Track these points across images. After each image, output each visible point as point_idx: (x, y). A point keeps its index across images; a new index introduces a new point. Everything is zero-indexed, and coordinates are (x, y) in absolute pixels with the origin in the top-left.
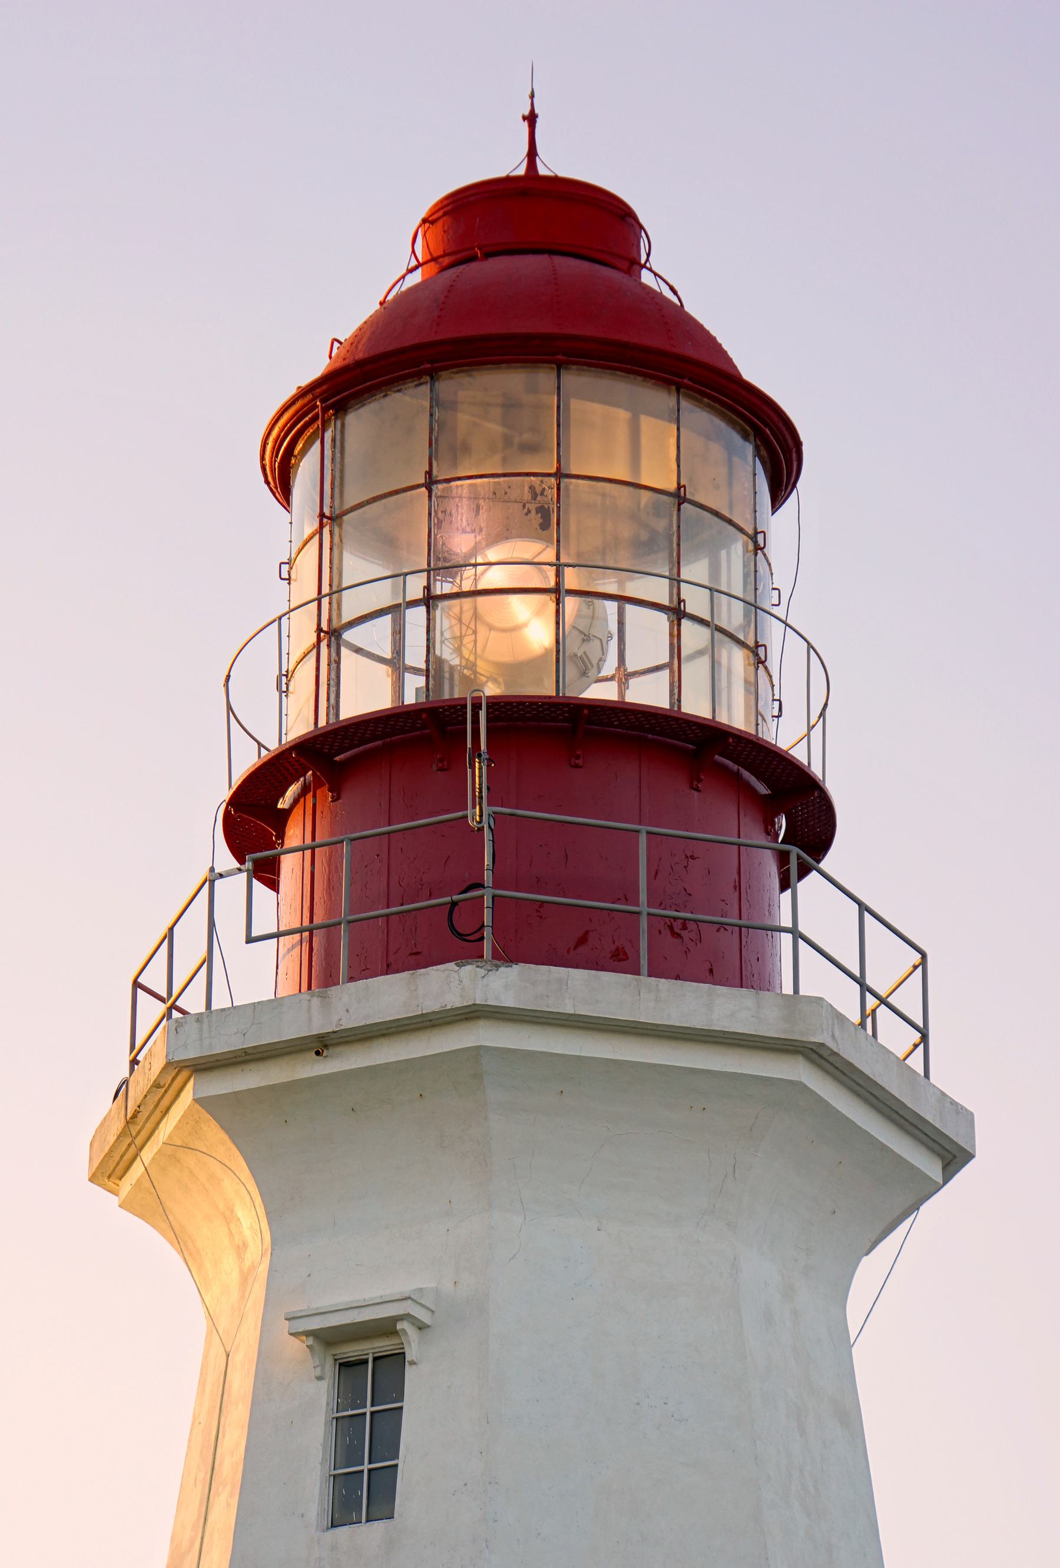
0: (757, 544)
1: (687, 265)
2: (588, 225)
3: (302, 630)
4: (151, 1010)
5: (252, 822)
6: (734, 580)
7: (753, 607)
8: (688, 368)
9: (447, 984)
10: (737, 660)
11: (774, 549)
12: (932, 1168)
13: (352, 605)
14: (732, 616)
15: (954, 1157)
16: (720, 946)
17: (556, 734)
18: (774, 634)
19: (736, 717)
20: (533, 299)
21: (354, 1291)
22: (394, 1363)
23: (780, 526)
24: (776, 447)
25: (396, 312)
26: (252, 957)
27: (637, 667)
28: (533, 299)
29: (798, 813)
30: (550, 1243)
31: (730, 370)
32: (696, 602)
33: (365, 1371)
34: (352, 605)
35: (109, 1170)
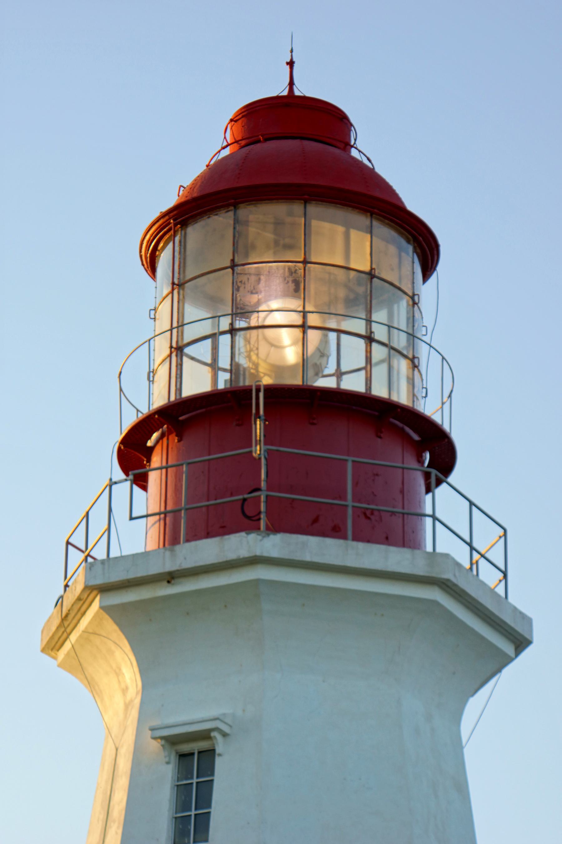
0: (414, 302)
1: (375, 146)
4: (76, 557)
5: (133, 454)
6: (401, 321)
7: (412, 336)
8: (373, 201)
10: (403, 365)
13: (190, 333)
14: (400, 341)
16: (393, 524)
17: (300, 405)
18: (423, 351)
19: (402, 397)
20: (291, 162)
21: (188, 715)
22: (208, 756)
24: (425, 247)
25: (216, 171)
26: (132, 525)
27: (348, 368)
28: (291, 162)
29: (436, 450)
32: (380, 333)
34: (190, 333)
35: (52, 646)
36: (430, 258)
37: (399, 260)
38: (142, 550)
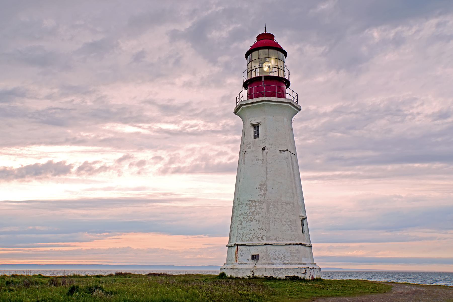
0: (284, 62)
1: (277, 40)
2: (271, 37)
3: (249, 70)
4: (238, 100)
5: (245, 85)
6: (282, 65)
7: (284, 67)
8: (279, 49)
9: (261, 99)
10: (282, 71)
11: (286, 63)
12: (298, 111)
13: (253, 68)
14: (282, 68)
15: (300, 110)
16: (282, 95)
17: (269, 79)
18: (285, 69)
19: (282, 76)
20: (266, 43)
22: (258, 127)
23: (285, 60)
24: (285, 54)
25: (255, 44)
29: (288, 84)
30: (267, 114)
31: (278, 47)
32: (279, 67)
33: (256, 127)
34: (253, 68)
35: (235, 112)
36: (349, 173)
37: (282, 55)
38: (260, 51)
